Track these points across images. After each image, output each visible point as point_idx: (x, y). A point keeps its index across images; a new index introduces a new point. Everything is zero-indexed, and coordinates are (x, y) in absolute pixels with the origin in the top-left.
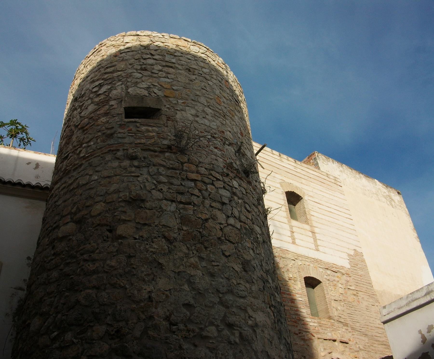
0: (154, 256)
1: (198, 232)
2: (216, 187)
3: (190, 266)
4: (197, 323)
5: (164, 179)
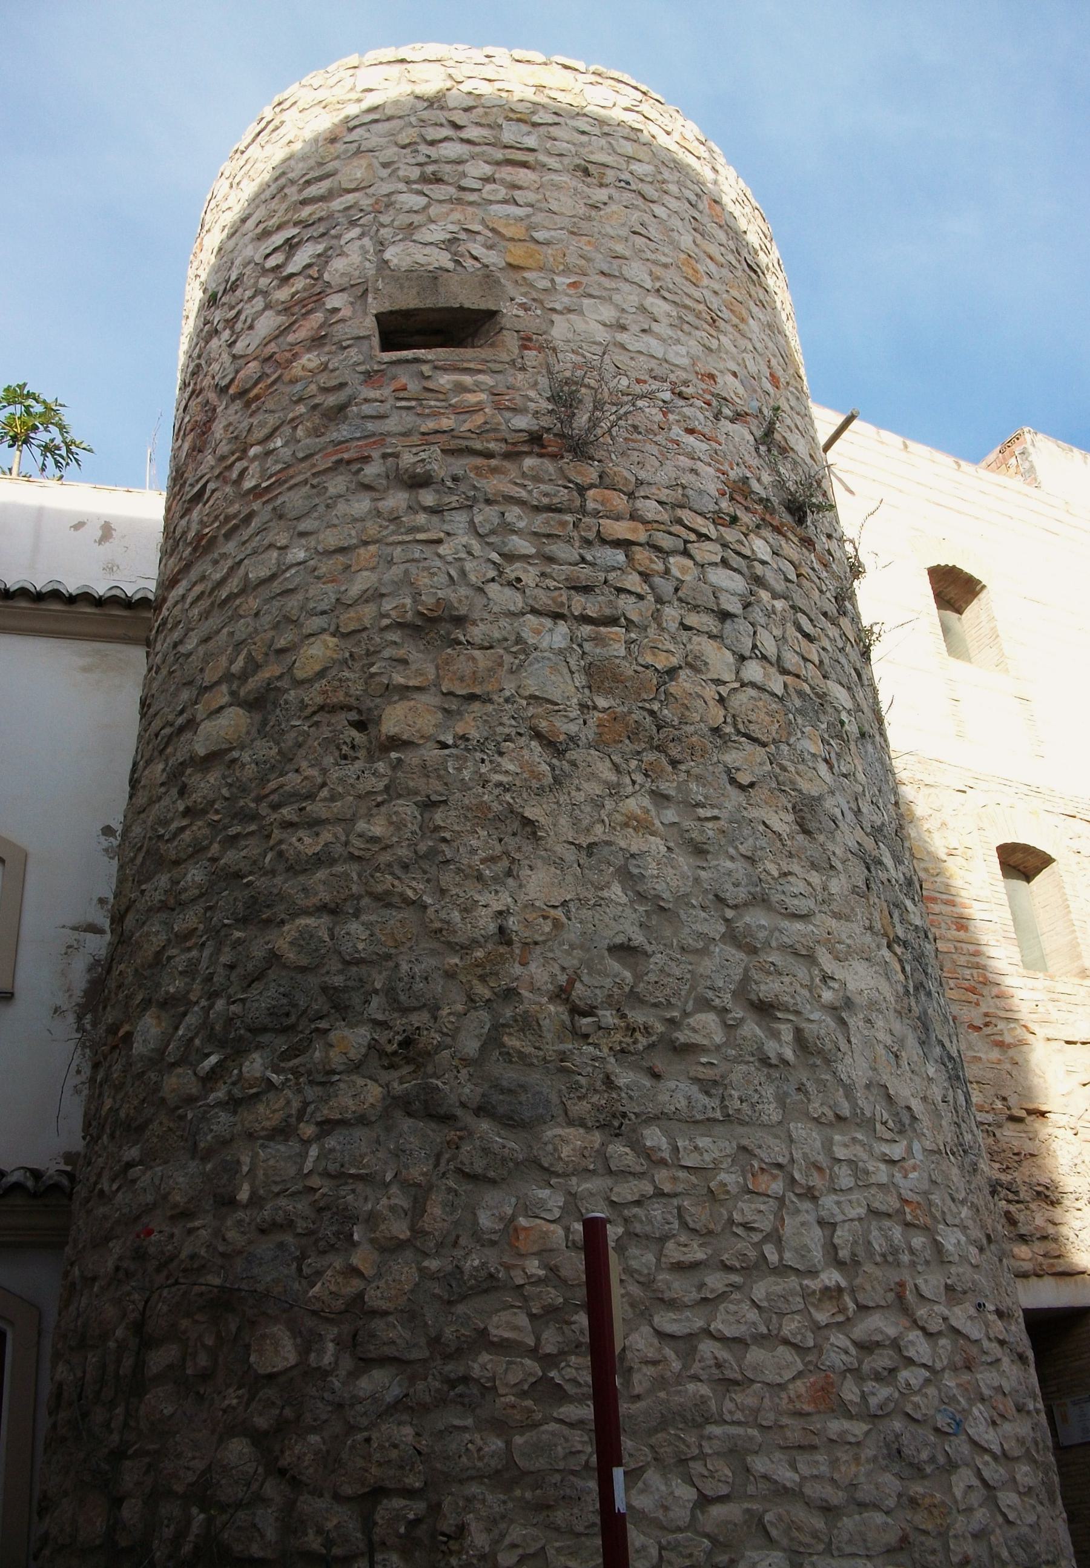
0: (508, 797)
1: (645, 714)
2: (696, 563)
3: (626, 825)
4: (655, 1005)
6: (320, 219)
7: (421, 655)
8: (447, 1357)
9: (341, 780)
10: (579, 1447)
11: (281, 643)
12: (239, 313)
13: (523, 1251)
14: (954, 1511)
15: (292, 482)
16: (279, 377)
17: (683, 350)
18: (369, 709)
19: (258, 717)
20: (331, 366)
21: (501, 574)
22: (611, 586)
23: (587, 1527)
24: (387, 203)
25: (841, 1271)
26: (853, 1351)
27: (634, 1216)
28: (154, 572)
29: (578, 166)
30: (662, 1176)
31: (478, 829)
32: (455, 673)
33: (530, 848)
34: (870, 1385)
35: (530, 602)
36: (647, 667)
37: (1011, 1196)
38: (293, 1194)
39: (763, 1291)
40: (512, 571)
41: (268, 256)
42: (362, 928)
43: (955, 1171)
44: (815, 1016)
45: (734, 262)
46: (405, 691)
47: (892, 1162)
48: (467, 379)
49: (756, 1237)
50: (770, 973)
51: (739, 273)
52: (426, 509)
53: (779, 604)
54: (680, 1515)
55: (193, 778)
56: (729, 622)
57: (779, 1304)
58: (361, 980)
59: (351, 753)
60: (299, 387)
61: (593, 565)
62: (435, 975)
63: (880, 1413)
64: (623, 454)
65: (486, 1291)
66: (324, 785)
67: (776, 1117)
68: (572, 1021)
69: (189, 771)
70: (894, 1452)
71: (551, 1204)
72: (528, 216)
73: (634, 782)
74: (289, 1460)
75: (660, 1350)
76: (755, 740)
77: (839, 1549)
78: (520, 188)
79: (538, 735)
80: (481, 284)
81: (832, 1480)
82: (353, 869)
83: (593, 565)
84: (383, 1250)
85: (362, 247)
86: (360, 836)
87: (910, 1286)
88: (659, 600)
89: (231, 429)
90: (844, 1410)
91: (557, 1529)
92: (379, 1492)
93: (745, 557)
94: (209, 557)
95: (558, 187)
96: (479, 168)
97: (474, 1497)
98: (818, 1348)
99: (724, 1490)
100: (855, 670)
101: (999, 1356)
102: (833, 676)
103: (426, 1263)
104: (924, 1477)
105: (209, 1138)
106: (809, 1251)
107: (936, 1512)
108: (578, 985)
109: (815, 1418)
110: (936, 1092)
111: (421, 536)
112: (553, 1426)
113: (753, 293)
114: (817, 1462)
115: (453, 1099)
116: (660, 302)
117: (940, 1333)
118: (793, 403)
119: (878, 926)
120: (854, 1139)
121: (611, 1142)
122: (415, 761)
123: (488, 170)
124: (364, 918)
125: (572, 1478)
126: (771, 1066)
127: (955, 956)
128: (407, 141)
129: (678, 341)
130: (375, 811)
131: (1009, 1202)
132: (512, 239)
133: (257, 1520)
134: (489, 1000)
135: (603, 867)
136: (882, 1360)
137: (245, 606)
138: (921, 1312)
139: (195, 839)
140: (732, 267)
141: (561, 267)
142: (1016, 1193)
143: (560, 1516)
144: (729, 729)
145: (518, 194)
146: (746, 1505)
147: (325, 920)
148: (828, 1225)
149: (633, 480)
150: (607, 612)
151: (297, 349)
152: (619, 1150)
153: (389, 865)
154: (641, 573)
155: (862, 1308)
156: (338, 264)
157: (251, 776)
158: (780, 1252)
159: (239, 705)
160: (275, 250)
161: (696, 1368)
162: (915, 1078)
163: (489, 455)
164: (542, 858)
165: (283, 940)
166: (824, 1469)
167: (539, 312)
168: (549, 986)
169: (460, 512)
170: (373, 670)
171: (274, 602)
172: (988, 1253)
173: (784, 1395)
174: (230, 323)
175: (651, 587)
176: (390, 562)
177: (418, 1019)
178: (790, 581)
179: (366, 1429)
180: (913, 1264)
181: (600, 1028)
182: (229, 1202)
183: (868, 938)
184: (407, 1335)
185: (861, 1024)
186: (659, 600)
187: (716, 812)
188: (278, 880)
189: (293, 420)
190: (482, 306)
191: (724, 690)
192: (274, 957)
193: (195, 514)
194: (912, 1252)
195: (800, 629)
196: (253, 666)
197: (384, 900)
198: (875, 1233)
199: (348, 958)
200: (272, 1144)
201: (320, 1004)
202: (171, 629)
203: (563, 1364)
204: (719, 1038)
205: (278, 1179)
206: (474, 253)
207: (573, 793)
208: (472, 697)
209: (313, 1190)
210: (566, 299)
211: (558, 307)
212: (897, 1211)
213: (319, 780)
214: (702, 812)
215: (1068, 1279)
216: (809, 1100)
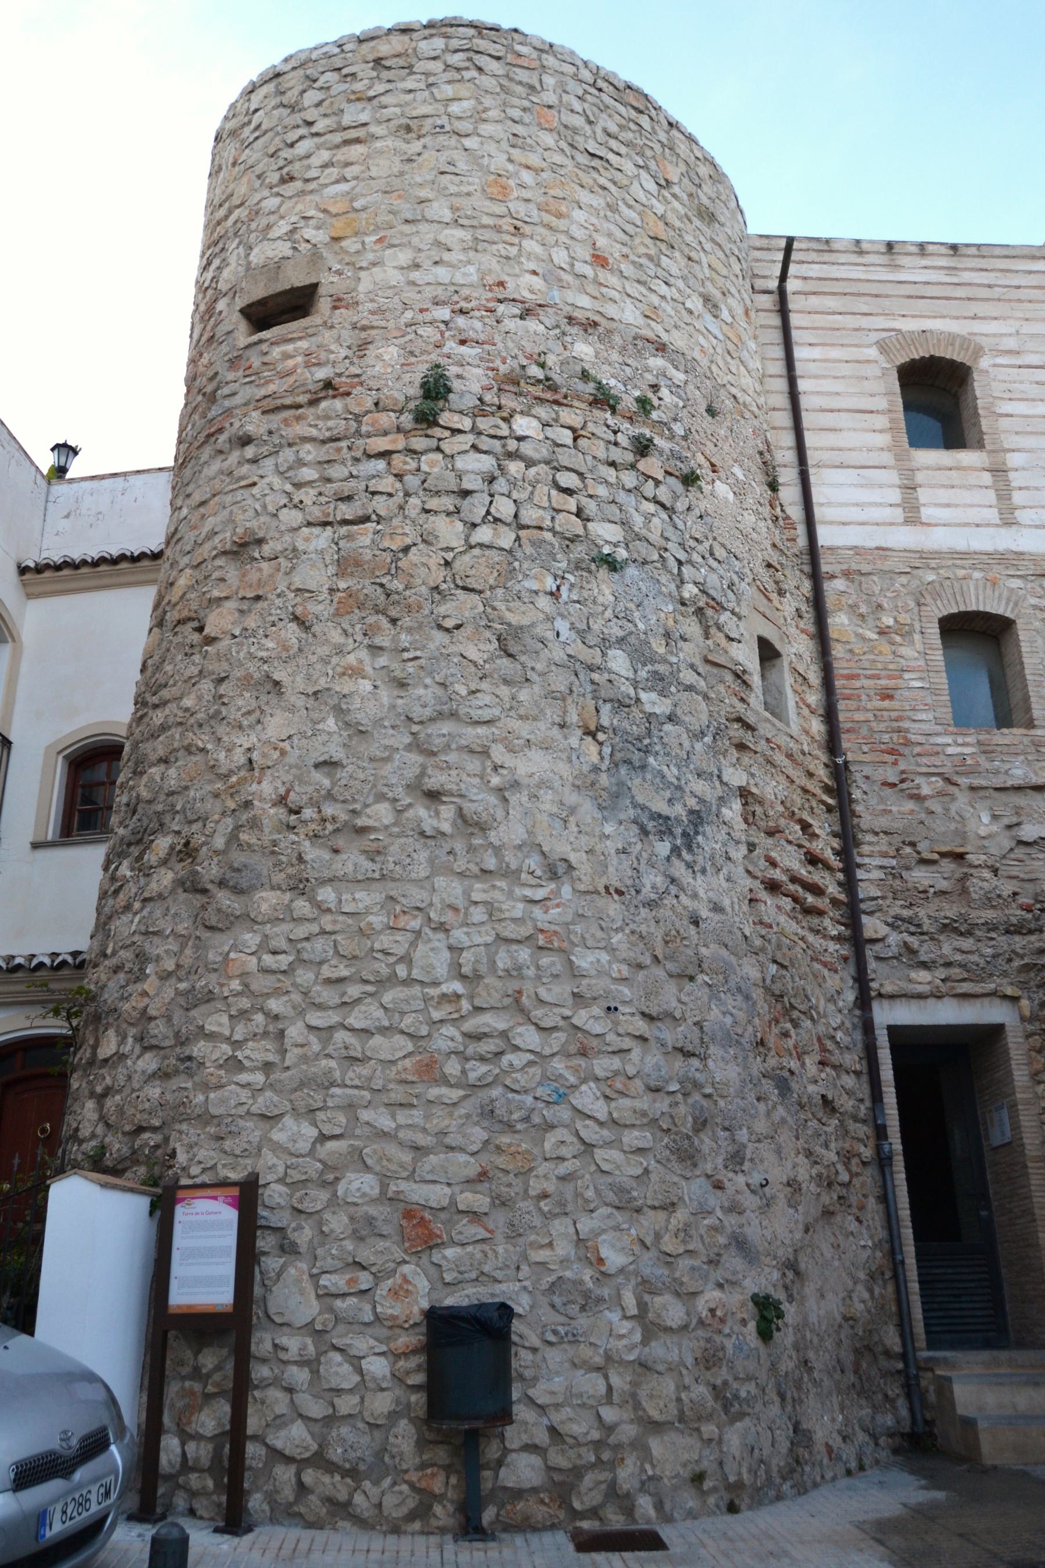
0: (265, 667)
1: (377, 587)
2: (446, 456)
3: (344, 674)
4: (344, 802)
5: (308, 474)
10: (244, 1100)
30: (327, 922)
37: (913, 929)
49: (392, 960)
54: (304, 1146)
61: (357, 477)
65: (208, 1001)
67: (423, 874)
79: (295, 618)
84: (161, 978)
90: (445, 1081)
112: (233, 1086)
127: (874, 724)
129: (469, 262)
136: (487, 1047)
138: (537, 1013)
143: (228, 1144)
148: (455, 950)
150: (360, 513)
152: (302, 906)
154: (396, 475)
161: (330, 1050)
163: (299, 406)
173: (394, 1069)
180: (539, 978)
187: (418, 653)
190: (307, 282)
197: (188, 749)
215: (972, 1001)
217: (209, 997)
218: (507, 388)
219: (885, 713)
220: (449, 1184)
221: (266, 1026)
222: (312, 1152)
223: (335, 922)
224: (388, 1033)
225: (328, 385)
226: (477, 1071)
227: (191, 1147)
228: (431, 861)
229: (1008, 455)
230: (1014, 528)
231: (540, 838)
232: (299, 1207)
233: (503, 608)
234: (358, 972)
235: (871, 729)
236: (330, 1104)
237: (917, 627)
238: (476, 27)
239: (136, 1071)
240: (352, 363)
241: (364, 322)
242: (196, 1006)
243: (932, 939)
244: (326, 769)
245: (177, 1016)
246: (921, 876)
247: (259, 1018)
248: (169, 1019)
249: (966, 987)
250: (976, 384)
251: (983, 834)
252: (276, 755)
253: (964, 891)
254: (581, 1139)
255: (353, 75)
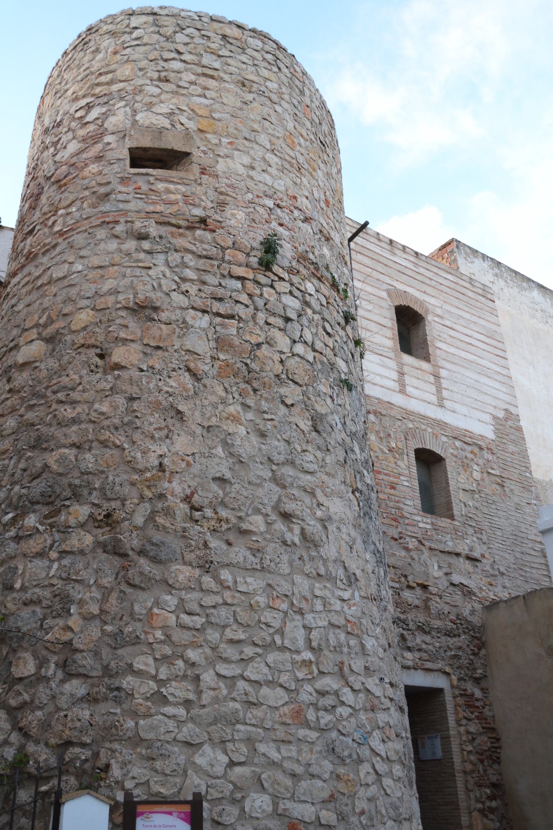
0: (171, 399)
1: (243, 365)
2: (276, 292)
3: (228, 418)
4: (233, 509)
6: (105, 95)
7: (135, 324)
8: (111, 676)
9: (89, 382)
10: (172, 729)
11: (66, 311)
12: (60, 139)
13: (154, 626)
14: (359, 785)
15: (79, 230)
16: (78, 175)
17: (282, 183)
18: (107, 349)
19: (50, 347)
20: (104, 173)
21: (179, 287)
22: (233, 299)
23: (172, 771)
24: (139, 90)
25: (312, 652)
26: (314, 694)
27: (212, 613)
28: (5, 268)
29: (239, 80)
30: (227, 594)
31: (155, 413)
32: (151, 335)
33: (179, 425)
34: (321, 713)
35: (192, 303)
36: (246, 342)
38: (43, 587)
39: (272, 658)
40: (185, 287)
41: (76, 111)
42: (91, 457)
43: (375, 608)
44: (312, 523)
45: (314, 139)
46: (125, 341)
47: (343, 600)
48: (172, 187)
49: (271, 631)
50: (291, 499)
51: (315, 145)
52: (144, 251)
53: (317, 317)
54: (219, 770)
55: (15, 374)
56: (290, 323)
57: (280, 666)
58: (88, 482)
59: (96, 370)
60: (86, 181)
61: (225, 288)
62: (126, 484)
63: (325, 728)
64: (246, 233)
65: (134, 644)
66: (80, 384)
67: (287, 571)
68: (191, 512)
69: (13, 370)
70: (331, 749)
71: (170, 603)
72: (211, 105)
73: (234, 398)
74: (25, 723)
75: (217, 683)
76: (296, 383)
77: (298, 797)
78: (208, 89)
79: (189, 370)
80: (183, 138)
81: (298, 760)
82: (91, 427)
83: (225, 288)
84: (85, 619)
85: (125, 112)
86: (95, 411)
87: (346, 664)
88: (256, 309)
89: (50, 199)
90: (307, 724)
91: (156, 771)
92: (68, 744)
93: (301, 291)
94: (34, 263)
95: (228, 91)
96: (189, 77)
97: (116, 750)
98: (297, 691)
99: (243, 759)
100: (351, 353)
101: (389, 706)
102: (339, 355)
103: (105, 627)
104: (345, 765)
105: (4, 555)
106: (297, 641)
107: (349, 784)
108: (195, 495)
109: (291, 727)
110: (369, 568)
111: (140, 264)
112: (160, 717)
113: (321, 156)
114: (291, 750)
115: (128, 546)
116: (273, 157)
117: (359, 690)
118: (335, 215)
119: (348, 481)
120: (325, 586)
121: (204, 575)
122: (127, 377)
123: (193, 78)
124: (93, 452)
125: (166, 744)
126: (287, 545)
127: (388, 502)
128: (153, 58)
129: (280, 178)
130: (104, 399)
131: (404, 629)
132: (201, 116)
133: (4, 754)
134: (151, 499)
135: (214, 438)
136: (329, 701)
137: (50, 290)
138: (351, 679)
139: (13, 404)
140: (312, 142)
141: (225, 133)
142: (407, 625)
143: (158, 764)
144: (284, 376)
145: (207, 93)
146: (253, 769)
147: (74, 451)
148: (308, 629)
149: (250, 246)
150: (230, 312)
151: (87, 161)
152: (207, 580)
153: (109, 427)
154: (248, 294)
155: (321, 673)
156: (112, 120)
157: (44, 376)
158: (283, 640)
159: (41, 340)
160: (81, 108)
162: (359, 559)
163: (179, 227)
164: (184, 430)
165: (51, 459)
166: (294, 754)
167: (211, 156)
168: (182, 495)
169: (161, 254)
170: (110, 329)
171: (64, 290)
172: (388, 653)
173: (277, 713)
174: (55, 144)
175: (253, 302)
176: (124, 276)
177: (113, 504)
178: (323, 305)
179: (66, 710)
180: (349, 654)
181: (204, 518)
182: (10, 588)
183: (343, 487)
184: (92, 662)
185: (334, 529)
186: (256, 309)
187: (273, 417)
188: (52, 429)
189: (82, 198)
190: (183, 150)
191: (283, 357)
192: (46, 466)
193: (28, 241)
194: (349, 647)
195: (325, 330)
196: (50, 321)
197: (104, 444)
198: (331, 635)
199: (83, 471)
200: (35, 560)
201: (67, 493)
202: (11, 298)
203: (168, 685)
204: (263, 528)
205: (36, 578)
206: (182, 121)
207: (203, 400)
208: (158, 348)
209: (53, 585)
210: (226, 150)
211: (222, 154)
212: (344, 626)
213: (78, 381)
214: (266, 416)
215: (430, 673)
216: (304, 564)
217: (136, 641)
218: (302, 261)
219: (393, 497)
220: (313, 804)
221: (185, 671)
222: (225, 776)
223: (233, 597)
224: (271, 685)
225: (203, 221)
226: (326, 718)
227: (125, 764)
228: (291, 563)
229: (441, 370)
230: (443, 409)
231: (344, 557)
232: (219, 820)
233: (314, 399)
234: (250, 637)
235: (387, 505)
236: (236, 737)
237: (405, 451)
238: (277, 44)
239: (62, 693)
240: (217, 213)
241: (223, 190)
242: (123, 647)
243: (412, 634)
244: (218, 483)
245: (105, 652)
246: (407, 595)
247: (180, 663)
248: (96, 654)
249: (429, 665)
250: (426, 327)
251: (436, 576)
252: (183, 465)
253: (427, 608)
254: (376, 771)
255: (208, 37)
